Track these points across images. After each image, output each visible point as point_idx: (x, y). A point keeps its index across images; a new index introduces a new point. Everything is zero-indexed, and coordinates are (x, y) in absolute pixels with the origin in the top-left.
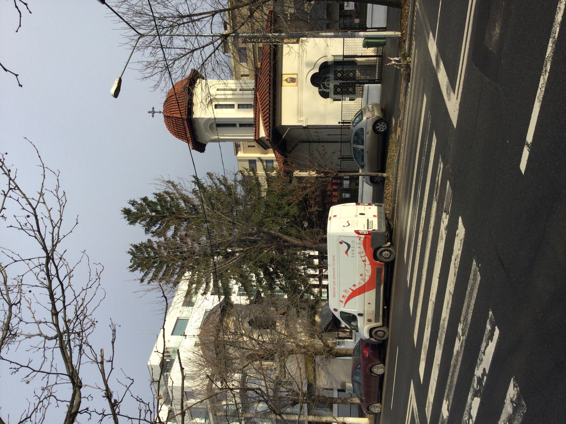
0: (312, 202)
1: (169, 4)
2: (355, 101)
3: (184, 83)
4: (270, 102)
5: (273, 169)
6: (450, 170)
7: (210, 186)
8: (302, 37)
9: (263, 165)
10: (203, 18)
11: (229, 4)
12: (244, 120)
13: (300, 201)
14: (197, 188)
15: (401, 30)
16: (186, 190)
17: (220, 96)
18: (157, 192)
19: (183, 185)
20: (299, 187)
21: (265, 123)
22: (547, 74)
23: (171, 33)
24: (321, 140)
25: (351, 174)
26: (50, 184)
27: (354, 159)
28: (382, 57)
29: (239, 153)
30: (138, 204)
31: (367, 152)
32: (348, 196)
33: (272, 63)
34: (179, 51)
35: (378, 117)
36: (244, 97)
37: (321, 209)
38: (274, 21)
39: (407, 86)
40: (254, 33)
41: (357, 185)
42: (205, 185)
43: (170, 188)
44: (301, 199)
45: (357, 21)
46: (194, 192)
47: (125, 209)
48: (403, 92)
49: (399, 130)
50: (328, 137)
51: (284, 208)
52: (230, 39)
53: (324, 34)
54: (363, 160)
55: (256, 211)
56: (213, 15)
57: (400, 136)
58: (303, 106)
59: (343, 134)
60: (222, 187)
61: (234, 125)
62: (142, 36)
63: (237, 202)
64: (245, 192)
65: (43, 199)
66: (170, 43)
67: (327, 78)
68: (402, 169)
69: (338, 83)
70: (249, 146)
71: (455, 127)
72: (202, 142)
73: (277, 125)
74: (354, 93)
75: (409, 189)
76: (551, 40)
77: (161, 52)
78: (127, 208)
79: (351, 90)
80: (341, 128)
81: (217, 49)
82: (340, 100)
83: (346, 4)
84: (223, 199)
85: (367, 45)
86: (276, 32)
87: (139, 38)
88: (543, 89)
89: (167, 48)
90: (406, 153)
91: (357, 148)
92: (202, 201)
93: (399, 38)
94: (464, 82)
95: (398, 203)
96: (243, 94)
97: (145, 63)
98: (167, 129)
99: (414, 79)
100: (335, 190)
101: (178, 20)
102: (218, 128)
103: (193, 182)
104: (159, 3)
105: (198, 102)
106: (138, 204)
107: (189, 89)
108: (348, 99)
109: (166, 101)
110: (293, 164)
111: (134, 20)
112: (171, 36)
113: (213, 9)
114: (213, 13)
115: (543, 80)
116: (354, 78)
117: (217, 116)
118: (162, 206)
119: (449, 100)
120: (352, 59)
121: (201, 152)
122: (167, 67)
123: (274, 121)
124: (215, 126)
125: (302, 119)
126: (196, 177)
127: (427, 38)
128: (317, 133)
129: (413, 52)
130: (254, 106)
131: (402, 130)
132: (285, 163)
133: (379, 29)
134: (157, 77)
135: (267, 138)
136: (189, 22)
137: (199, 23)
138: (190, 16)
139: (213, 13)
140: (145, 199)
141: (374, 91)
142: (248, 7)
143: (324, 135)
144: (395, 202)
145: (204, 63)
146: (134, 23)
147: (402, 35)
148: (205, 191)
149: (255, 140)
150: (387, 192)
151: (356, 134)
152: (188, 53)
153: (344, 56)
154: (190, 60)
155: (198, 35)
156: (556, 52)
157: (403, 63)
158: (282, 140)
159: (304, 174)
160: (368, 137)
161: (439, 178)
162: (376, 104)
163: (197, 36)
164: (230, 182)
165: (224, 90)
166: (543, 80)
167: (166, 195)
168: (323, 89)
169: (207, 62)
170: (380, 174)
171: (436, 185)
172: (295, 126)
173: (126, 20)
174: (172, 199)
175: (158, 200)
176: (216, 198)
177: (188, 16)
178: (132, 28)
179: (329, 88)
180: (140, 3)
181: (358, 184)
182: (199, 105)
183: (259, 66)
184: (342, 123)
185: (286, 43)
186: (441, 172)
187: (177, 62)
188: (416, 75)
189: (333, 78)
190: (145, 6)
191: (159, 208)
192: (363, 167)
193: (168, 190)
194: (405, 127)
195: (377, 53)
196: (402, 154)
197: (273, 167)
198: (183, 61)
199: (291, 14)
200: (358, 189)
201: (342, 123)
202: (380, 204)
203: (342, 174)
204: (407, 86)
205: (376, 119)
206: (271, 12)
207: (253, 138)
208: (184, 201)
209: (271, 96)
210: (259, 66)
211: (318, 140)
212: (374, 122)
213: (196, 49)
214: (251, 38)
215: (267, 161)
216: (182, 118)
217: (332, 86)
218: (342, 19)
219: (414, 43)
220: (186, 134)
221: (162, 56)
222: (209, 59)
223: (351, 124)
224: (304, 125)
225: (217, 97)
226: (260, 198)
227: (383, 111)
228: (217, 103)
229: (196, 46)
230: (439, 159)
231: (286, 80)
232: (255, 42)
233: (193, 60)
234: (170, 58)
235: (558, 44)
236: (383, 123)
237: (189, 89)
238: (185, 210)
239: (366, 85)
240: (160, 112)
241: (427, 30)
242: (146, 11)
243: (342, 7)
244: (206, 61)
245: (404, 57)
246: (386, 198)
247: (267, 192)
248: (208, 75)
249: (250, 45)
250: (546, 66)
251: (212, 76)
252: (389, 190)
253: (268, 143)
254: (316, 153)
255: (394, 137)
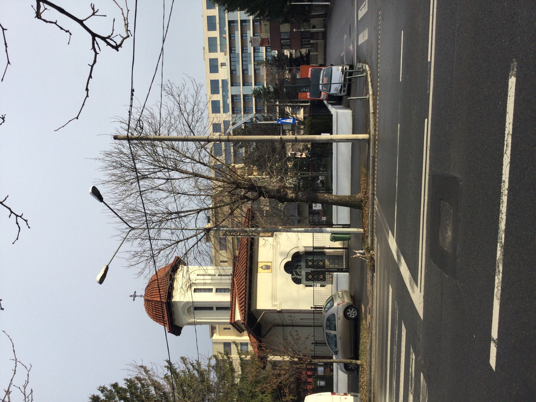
0: (286, 391)
1: (160, 203)
2: (326, 287)
3: (167, 270)
4: (246, 287)
5: (247, 353)
6: (423, 362)
7: (183, 371)
8: (276, 231)
9: (238, 350)
10: (189, 215)
11: (213, 203)
12: (221, 304)
13: (274, 390)
14: (169, 374)
15: (363, 227)
16: (158, 376)
17: (201, 281)
18: (129, 378)
19: (156, 371)
20: (273, 374)
21: (241, 307)
22: (501, 274)
23: (159, 226)
24: (295, 324)
25: (325, 361)
26: (19, 380)
27: (328, 345)
28: (348, 249)
29: (215, 335)
30: (107, 391)
31: (340, 338)
32: (322, 383)
33: (249, 253)
34: (165, 242)
35: (348, 303)
36: (222, 281)
37: (296, 398)
38: (251, 217)
39: (373, 275)
40: (233, 227)
41: (332, 370)
42: (178, 371)
43: (142, 374)
44: (275, 387)
45: (324, 219)
46: (166, 377)
47: (93, 396)
48: (369, 281)
49: (369, 317)
50: (302, 321)
51: (258, 396)
52: (212, 233)
53: (295, 229)
54: (336, 346)
55: (229, 399)
56: (198, 213)
57: (370, 323)
58: (277, 292)
59: (316, 318)
60: (195, 372)
61: (211, 308)
62: (133, 229)
63: (209, 390)
64: (219, 378)
65: (9, 398)
66: (158, 235)
67: (299, 266)
68: (376, 357)
69: (309, 270)
70: (224, 329)
71: (422, 318)
72: (178, 325)
73: (253, 309)
74: (324, 279)
75: (384, 380)
76: (499, 244)
77: (149, 243)
78: (96, 395)
79: (321, 277)
80: (314, 312)
81: (200, 240)
82: (311, 286)
83: (314, 205)
84: (195, 386)
85: (334, 239)
86: (253, 227)
87: (130, 231)
88: (500, 288)
89: (154, 239)
90: (377, 341)
91: (330, 334)
92: (173, 389)
93: (362, 234)
94: (425, 277)
95: (374, 393)
96: (221, 279)
97: (133, 253)
98: (146, 312)
99: (379, 270)
100: (309, 376)
101: (167, 216)
102: (195, 312)
103: (165, 367)
104: (151, 202)
105: (179, 287)
106: (107, 391)
107: (171, 276)
108: (319, 285)
109: (148, 286)
110: (267, 349)
111: (127, 216)
112: (160, 229)
113: (198, 208)
114: (198, 211)
115: (498, 279)
116: (323, 266)
117: (195, 300)
118: (132, 394)
119: (413, 292)
120: (321, 250)
121: (177, 335)
122: (153, 256)
123: (250, 305)
124: (192, 309)
125: (276, 303)
126: (169, 362)
127: (387, 235)
128: (291, 316)
129: (375, 246)
130: (231, 290)
131: (372, 317)
132: (260, 347)
133: (344, 226)
134: (142, 265)
135: (242, 321)
136: (176, 218)
137: (186, 218)
138: (178, 213)
139: (198, 211)
140: (115, 386)
141: (342, 279)
142: (229, 206)
143: (297, 319)
144: (371, 392)
145: (187, 253)
146: (127, 218)
147: (365, 231)
148: (177, 378)
149: (230, 323)
150: (362, 380)
151: (328, 319)
152: (174, 244)
153: (314, 248)
154: (174, 250)
155: (183, 229)
156: (505, 254)
157: (368, 255)
158: (257, 324)
159: (278, 358)
160: (340, 322)
161: (413, 369)
162: (346, 292)
163: (182, 229)
164: (204, 367)
165: (204, 275)
166: (498, 279)
167: (137, 382)
168: (295, 276)
169: (190, 252)
170: (354, 361)
171: (410, 376)
172: (269, 310)
173: (120, 216)
174: (143, 385)
175: (128, 386)
176: (188, 384)
177: (176, 213)
178: (125, 222)
179: (301, 275)
180: (135, 202)
181: (333, 370)
182: (179, 290)
183: (237, 255)
184: (314, 308)
185: (261, 237)
186: (413, 363)
187: (162, 252)
188: (380, 267)
189: (305, 267)
190: (138, 204)
191: (128, 394)
192: (336, 353)
193: (140, 375)
194: (375, 314)
195: (344, 245)
196: (374, 341)
197: (247, 352)
198: (168, 251)
199: (266, 211)
200: (333, 375)
201: (314, 308)
202: (356, 394)
203: (316, 361)
204: (373, 277)
205: (346, 306)
206: (249, 210)
207: (229, 321)
208: (155, 388)
209: (248, 281)
210: (237, 255)
211: (291, 324)
212: (344, 308)
213: (181, 241)
214: (230, 232)
215: (242, 344)
216: (161, 302)
217: (303, 273)
218: (311, 215)
219: (376, 238)
220: (164, 317)
221: (150, 246)
222: (192, 249)
223: (323, 309)
224: (278, 310)
225: (197, 281)
226: (233, 385)
227: (352, 297)
228: (196, 287)
229: (181, 238)
230: (410, 350)
231: (262, 267)
232: (234, 235)
233: (177, 250)
234: (156, 248)
235: (506, 248)
236: (353, 309)
237: (171, 276)
238: (155, 398)
239: (335, 273)
240: (141, 296)
241: (386, 229)
242: (139, 208)
243: (311, 207)
244: (189, 250)
245: (368, 250)
246: (361, 387)
247: (241, 379)
248: (190, 264)
249: (230, 238)
250: (498, 267)
251: (193, 264)
252: (364, 379)
253: (243, 327)
254: (290, 338)
255: (364, 324)
